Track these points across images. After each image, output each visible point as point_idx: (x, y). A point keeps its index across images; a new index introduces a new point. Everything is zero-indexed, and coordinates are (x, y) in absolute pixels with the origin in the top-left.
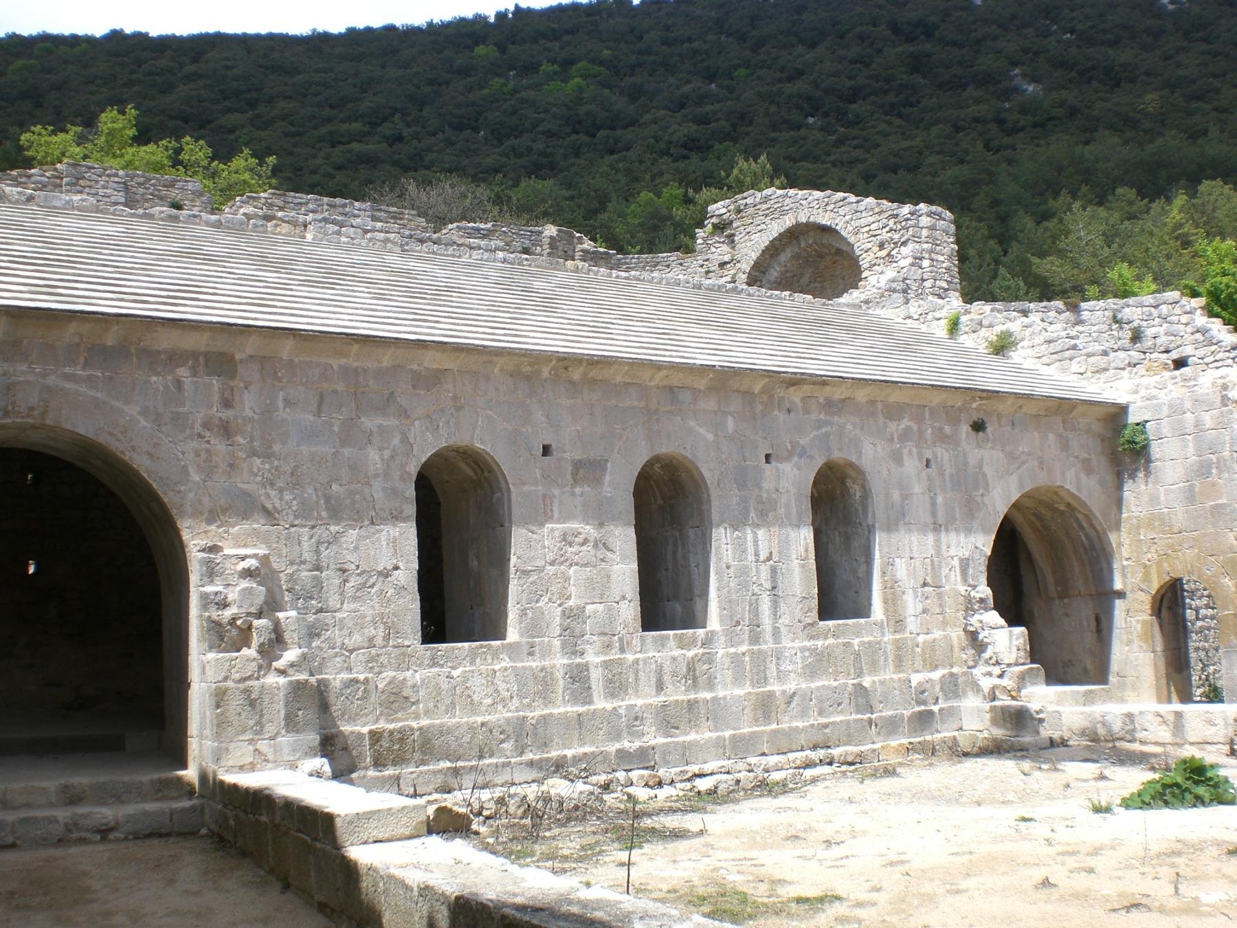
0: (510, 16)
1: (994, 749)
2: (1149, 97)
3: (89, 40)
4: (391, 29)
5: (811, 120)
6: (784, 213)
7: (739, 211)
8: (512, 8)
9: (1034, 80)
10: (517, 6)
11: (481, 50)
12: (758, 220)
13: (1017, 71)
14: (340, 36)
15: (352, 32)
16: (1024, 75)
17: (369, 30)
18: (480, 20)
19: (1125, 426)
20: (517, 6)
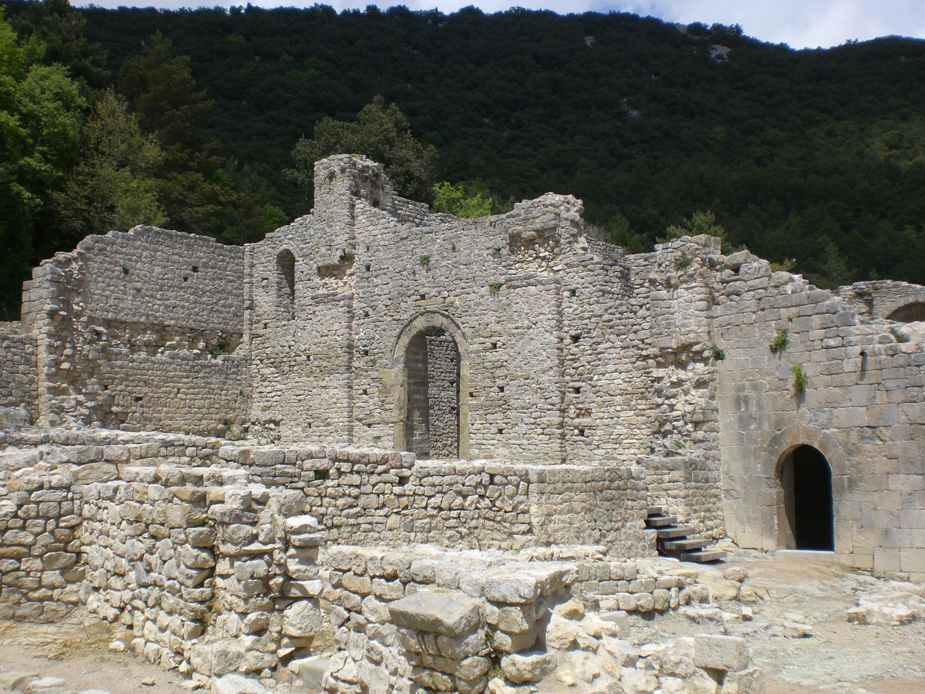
0: (243, 11)
1: (458, 414)
2: (718, 129)
3: (209, 11)
4: (152, 10)
5: (487, 120)
6: (908, 295)
7: (877, 289)
8: (245, 6)
9: (636, 107)
10: (249, 5)
11: (233, 38)
12: (890, 296)
13: (625, 100)
14: (113, 11)
15: (123, 10)
16: (629, 103)
17: (135, 10)
18: (219, 11)
19: (166, 161)
20: (249, 5)
